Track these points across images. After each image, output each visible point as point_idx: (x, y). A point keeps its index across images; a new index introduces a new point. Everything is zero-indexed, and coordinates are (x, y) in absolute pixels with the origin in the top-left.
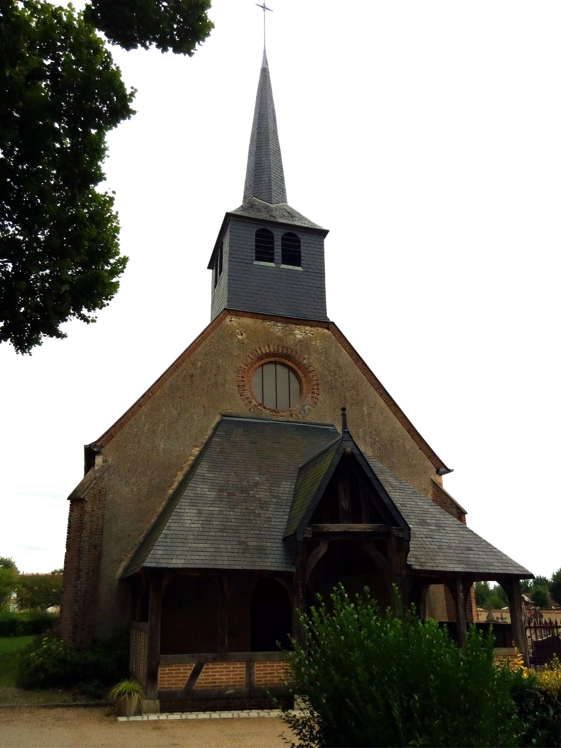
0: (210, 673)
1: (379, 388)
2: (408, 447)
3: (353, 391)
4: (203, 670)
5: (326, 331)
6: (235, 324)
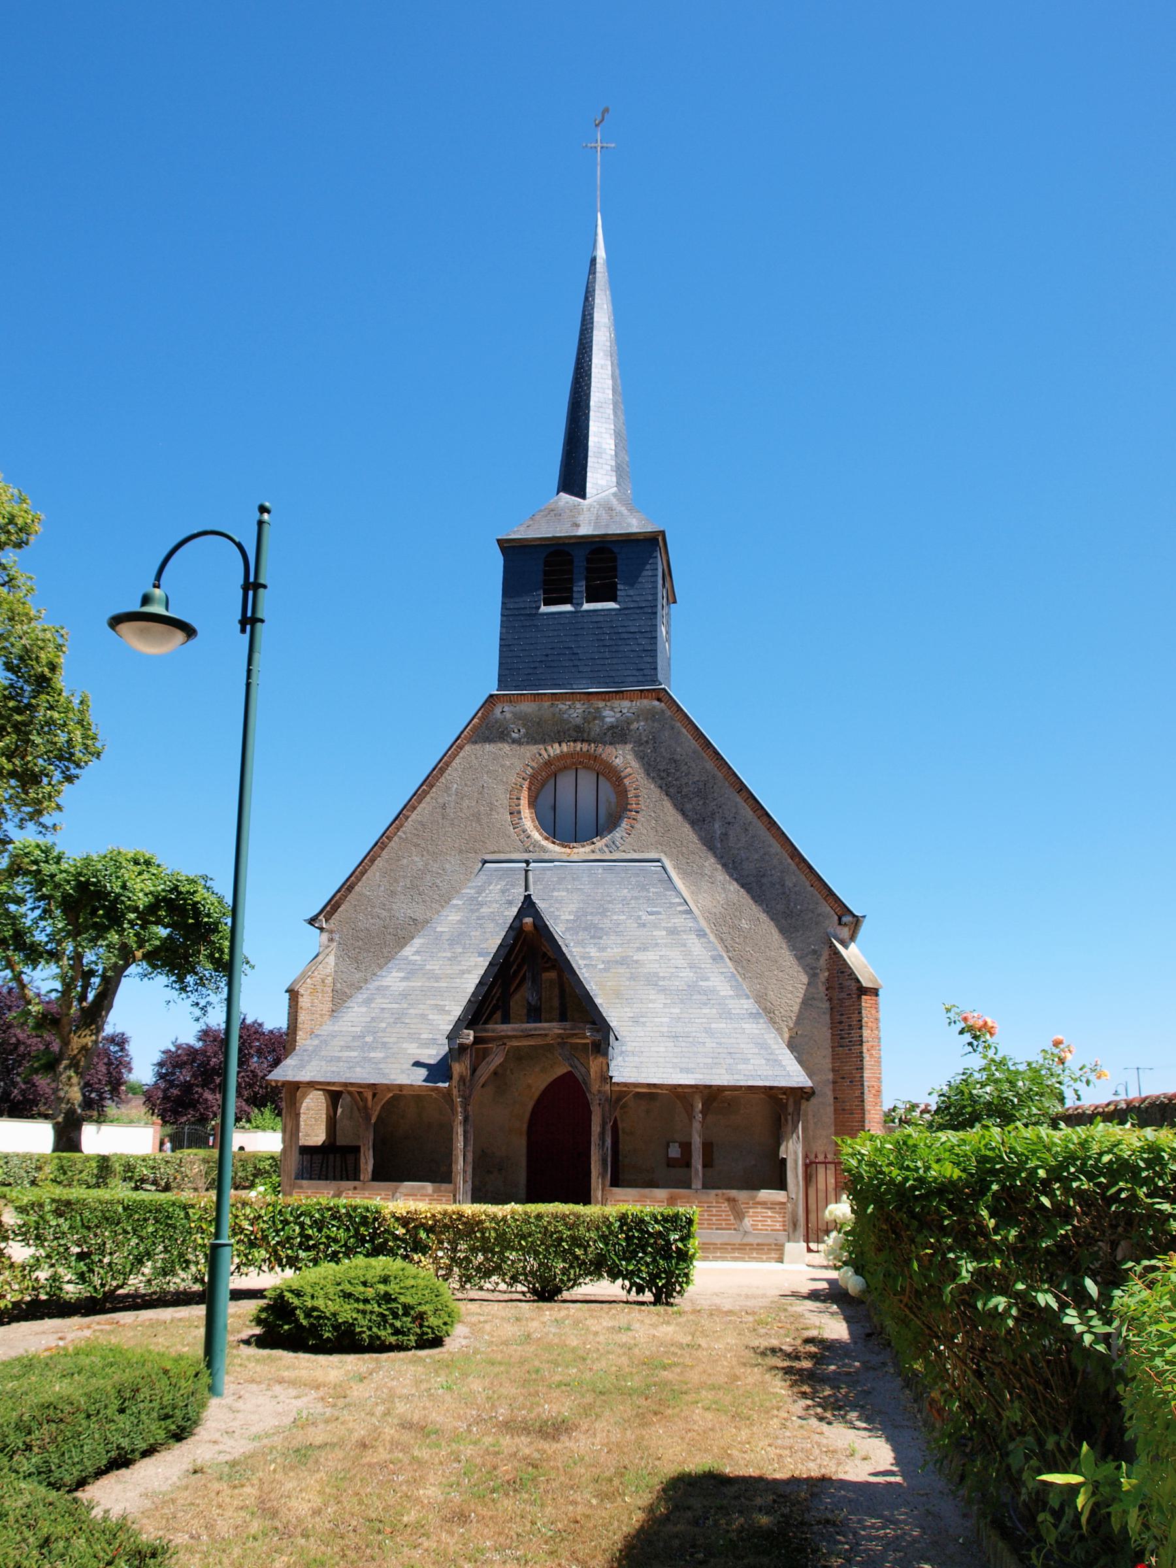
2: (789, 884)
5: (656, 703)
6: (508, 716)
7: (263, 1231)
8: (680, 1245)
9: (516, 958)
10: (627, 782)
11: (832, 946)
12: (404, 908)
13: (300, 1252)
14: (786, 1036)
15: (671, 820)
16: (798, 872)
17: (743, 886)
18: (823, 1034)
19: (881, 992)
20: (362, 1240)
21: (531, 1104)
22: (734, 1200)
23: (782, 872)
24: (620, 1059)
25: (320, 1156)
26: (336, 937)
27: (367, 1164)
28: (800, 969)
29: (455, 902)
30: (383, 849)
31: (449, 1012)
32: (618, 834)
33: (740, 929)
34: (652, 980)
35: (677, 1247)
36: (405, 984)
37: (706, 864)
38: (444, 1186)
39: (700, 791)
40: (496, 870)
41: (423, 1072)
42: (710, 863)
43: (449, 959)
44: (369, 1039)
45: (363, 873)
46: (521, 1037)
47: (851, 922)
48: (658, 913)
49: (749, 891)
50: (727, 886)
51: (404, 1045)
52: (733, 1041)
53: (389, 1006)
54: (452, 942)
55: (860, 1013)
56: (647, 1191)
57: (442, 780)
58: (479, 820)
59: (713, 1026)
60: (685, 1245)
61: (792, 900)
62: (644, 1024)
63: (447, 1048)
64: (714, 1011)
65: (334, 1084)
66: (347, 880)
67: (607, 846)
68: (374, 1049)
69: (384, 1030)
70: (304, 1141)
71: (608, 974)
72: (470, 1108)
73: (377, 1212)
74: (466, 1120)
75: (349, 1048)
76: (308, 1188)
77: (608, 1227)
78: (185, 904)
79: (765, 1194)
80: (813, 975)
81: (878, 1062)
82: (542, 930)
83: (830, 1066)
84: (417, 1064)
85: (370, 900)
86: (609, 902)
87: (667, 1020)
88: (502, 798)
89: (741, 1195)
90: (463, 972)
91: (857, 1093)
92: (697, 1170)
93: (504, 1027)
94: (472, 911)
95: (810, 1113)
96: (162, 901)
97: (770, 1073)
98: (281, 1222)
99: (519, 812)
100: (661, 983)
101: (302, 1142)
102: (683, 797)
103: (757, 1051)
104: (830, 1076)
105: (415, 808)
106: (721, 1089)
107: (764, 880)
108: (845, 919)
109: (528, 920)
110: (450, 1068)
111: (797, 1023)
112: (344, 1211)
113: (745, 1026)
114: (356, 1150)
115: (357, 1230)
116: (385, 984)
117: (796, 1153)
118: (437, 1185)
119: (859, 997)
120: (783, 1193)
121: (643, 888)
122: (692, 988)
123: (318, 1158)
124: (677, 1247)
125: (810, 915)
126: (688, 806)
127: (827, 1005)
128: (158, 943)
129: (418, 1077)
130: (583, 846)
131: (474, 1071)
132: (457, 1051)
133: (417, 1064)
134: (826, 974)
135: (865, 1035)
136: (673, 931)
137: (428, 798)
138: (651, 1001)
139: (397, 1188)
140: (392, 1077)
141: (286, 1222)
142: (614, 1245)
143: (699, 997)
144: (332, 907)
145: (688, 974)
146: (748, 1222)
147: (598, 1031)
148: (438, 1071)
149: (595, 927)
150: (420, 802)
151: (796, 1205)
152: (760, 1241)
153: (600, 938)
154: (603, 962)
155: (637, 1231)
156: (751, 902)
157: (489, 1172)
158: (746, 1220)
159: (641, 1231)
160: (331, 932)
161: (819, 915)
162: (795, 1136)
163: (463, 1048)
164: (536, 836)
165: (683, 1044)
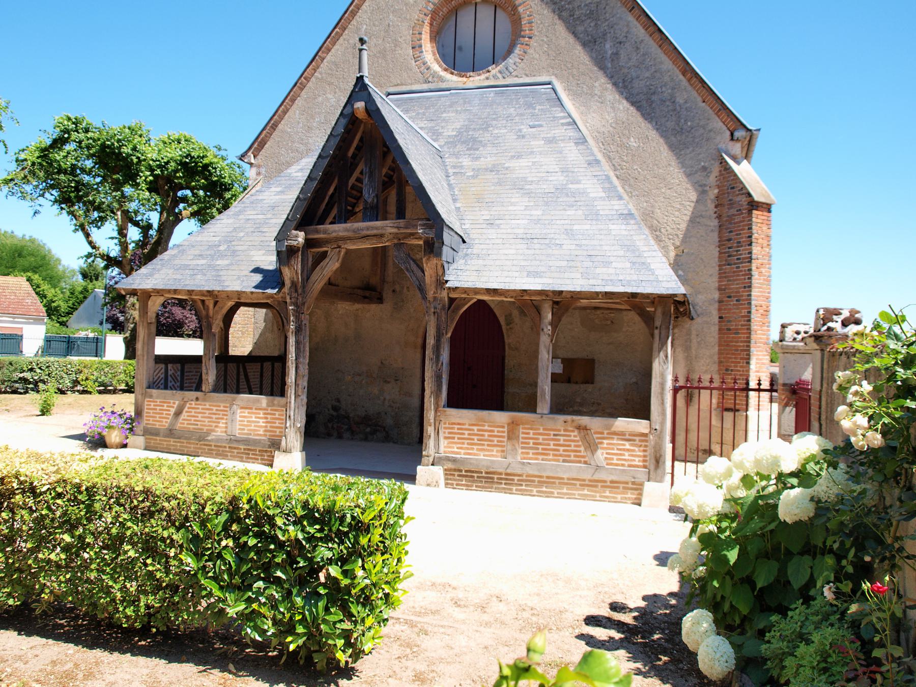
2: (680, 100)
4: (186, 409)
8: (335, 571)
10: (521, 9)
11: (723, 162)
14: (672, 254)
15: (563, 43)
16: (690, 88)
18: (712, 252)
19: (773, 209)
22: (586, 428)
23: (673, 89)
25: (179, 366)
26: (263, 170)
28: (689, 186)
30: (302, 89)
32: (510, 60)
33: (628, 148)
34: (520, 186)
35: (328, 576)
37: (597, 84)
38: (278, 400)
39: (592, 12)
42: (601, 83)
45: (285, 113)
47: (745, 138)
48: (541, 126)
49: (639, 108)
50: (616, 105)
52: (595, 242)
53: (255, 217)
57: (354, 22)
58: (384, 57)
59: (575, 227)
60: (345, 573)
61: (683, 112)
62: (498, 226)
64: (580, 212)
66: (271, 119)
67: (500, 72)
71: (475, 181)
77: (203, 524)
79: (623, 423)
80: (702, 191)
81: (768, 280)
83: (717, 285)
84: (257, 270)
86: (494, 119)
87: (526, 222)
88: (406, 34)
89: (594, 423)
91: (744, 312)
92: (543, 391)
95: (694, 333)
97: (635, 277)
99: (420, 46)
101: (157, 353)
102: (574, 20)
103: (621, 253)
104: (716, 295)
105: (329, 50)
106: (575, 296)
107: (654, 98)
108: (737, 134)
109: (360, 105)
111: (684, 240)
113: (612, 227)
121: (530, 106)
122: (561, 190)
124: (328, 576)
125: (701, 131)
126: (580, 29)
127: (715, 223)
130: (479, 75)
131: (307, 278)
134: (716, 191)
135: (754, 252)
136: (551, 141)
137: (341, 41)
138: (512, 204)
140: (226, 284)
143: (565, 199)
145: (560, 178)
147: (430, 227)
149: (474, 140)
150: (334, 44)
151: (660, 437)
152: (615, 478)
153: (477, 149)
155: (256, 535)
156: (640, 119)
157: (387, 382)
158: (599, 452)
160: (259, 166)
161: (710, 131)
162: (662, 354)
164: (436, 67)
165: (537, 246)
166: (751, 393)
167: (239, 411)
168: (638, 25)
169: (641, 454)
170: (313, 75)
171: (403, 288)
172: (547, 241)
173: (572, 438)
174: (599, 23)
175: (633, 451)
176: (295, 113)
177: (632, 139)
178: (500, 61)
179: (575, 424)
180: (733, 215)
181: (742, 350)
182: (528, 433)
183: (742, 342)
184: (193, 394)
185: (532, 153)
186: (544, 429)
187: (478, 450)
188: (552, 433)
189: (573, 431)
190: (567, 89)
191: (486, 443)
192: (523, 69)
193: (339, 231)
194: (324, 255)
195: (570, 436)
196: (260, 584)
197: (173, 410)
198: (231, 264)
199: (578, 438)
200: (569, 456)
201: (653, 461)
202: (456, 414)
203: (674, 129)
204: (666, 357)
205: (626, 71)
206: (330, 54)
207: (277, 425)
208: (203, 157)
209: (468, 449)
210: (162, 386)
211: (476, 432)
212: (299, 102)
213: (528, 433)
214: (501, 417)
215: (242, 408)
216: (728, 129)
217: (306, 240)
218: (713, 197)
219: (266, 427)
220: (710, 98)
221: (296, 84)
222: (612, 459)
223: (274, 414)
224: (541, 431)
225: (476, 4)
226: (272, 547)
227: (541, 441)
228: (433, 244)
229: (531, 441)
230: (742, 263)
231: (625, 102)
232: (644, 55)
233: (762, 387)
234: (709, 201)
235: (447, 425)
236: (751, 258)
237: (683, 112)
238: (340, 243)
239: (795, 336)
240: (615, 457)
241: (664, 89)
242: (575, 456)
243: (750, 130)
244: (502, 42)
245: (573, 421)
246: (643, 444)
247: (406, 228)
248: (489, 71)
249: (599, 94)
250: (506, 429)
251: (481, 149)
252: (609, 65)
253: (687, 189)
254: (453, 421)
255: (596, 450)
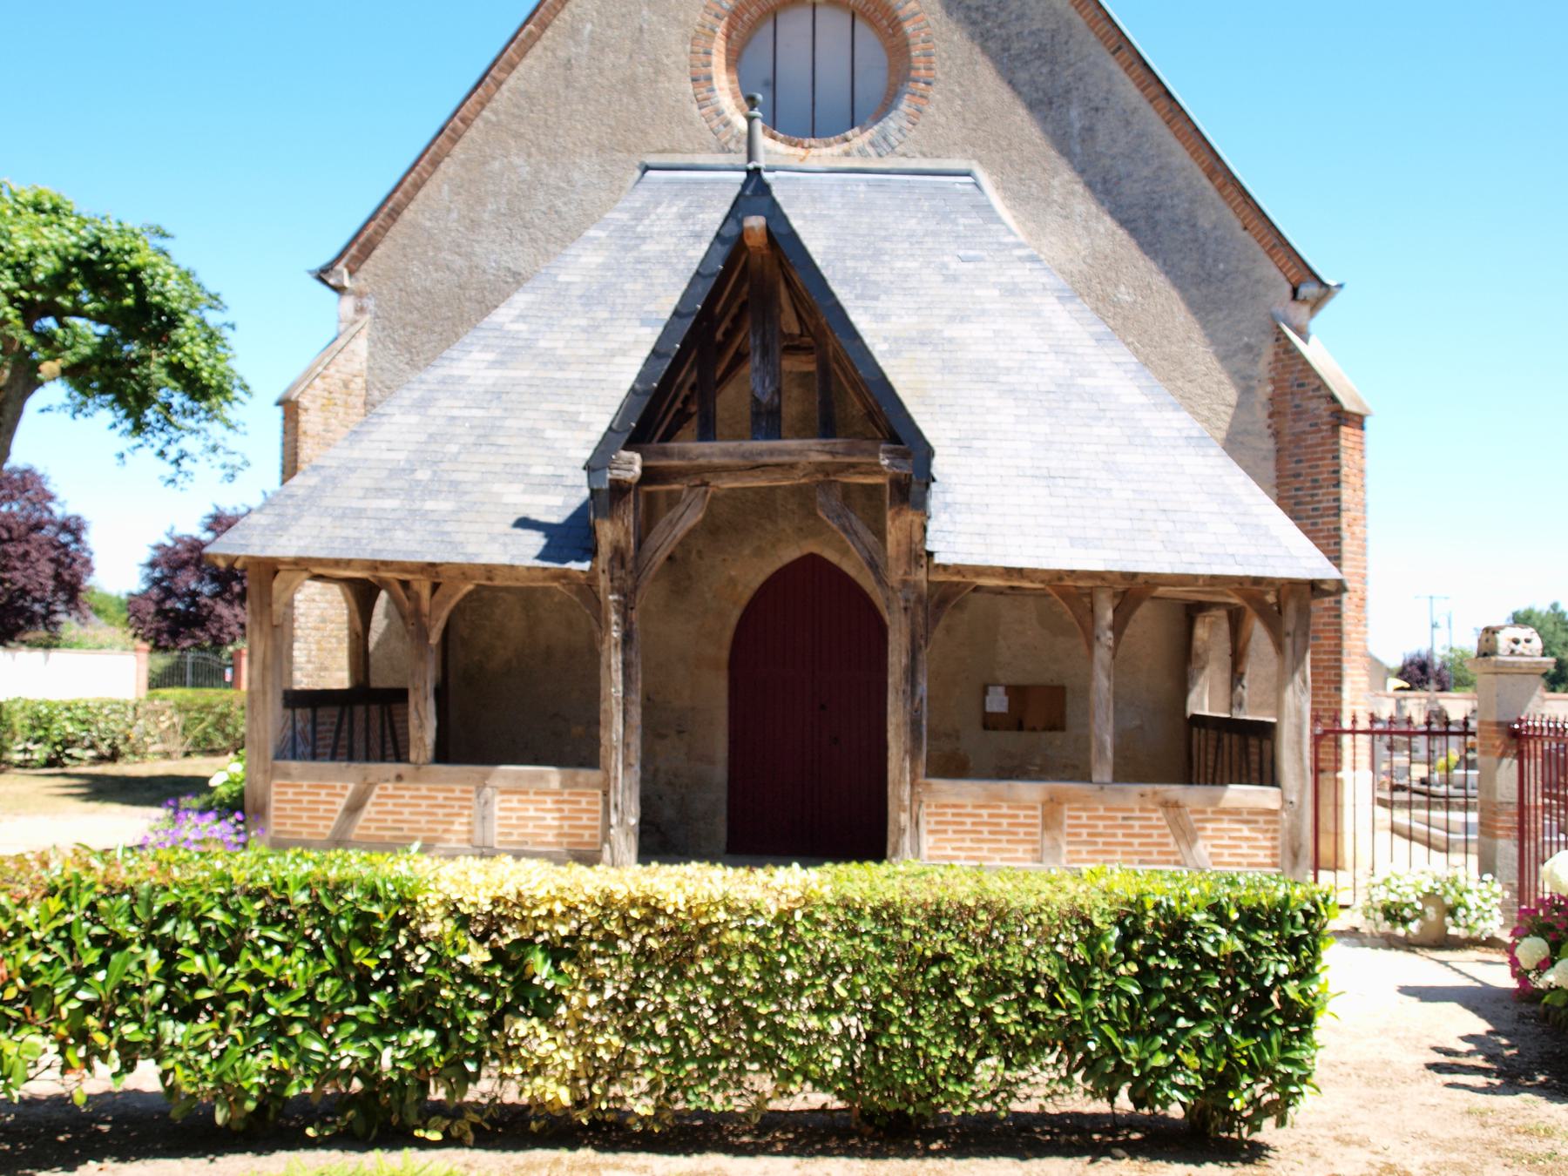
0: (390, 808)
1: (1119, 48)
2: (1204, 223)
3: (1038, 63)
4: (373, 799)
7: (28, 974)
9: (727, 305)
10: (909, 28)
11: (1281, 337)
12: (493, 253)
13: (168, 1026)
15: (990, 99)
16: (1221, 203)
17: (1123, 223)
19: (1368, 422)
20: (363, 986)
21: (735, 615)
22: (1176, 805)
23: (1192, 202)
24: (944, 517)
25: (336, 711)
26: (370, 304)
27: (423, 727)
28: (1223, 377)
29: (591, 233)
30: (454, 141)
31: (587, 426)
32: (892, 123)
33: (1116, 304)
36: (497, 373)
37: (1056, 182)
38: (584, 774)
39: (1043, 48)
40: (668, 182)
41: (537, 540)
42: (1064, 180)
43: (584, 330)
44: (423, 475)
45: (418, 186)
46: (740, 469)
48: (981, 259)
49: (1133, 232)
50: (1093, 224)
51: (497, 487)
53: (466, 413)
54: (588, 300)
55: (1337, 457)
56: (1001, 786)
57: (565, 15)
58: (633, 92)
61: (1210, 252)
63: (586, 493)
65: (348, 563)
66: (389, 197)
67: (872, 144)
68: (432, 494)
69: (454, 458)
70: (304, 680)
72: (634, 615)
73: (402, 901)
74: (627, 639)
75: (380, 491)
76: (302, 777)
78: (114, 271)
79: (1238, 794)
80: (1246, 391)
82: (783, 245)
84: (524, 523)
85: (431, 237)
86: (885, 239)
88: (677, 53)
90: (613, 354)
93: (706, 447)
94: (626, 249)
96: (73, 264)
98: (97, 941)
99: (709, 79)
100: (1003, 379)
105: (513, 66)
108: (1304, 291)
109: (756, 222)
110: (592, 532)
112: (303, 898)
114: (401, 695)
115: (343, 957)
116: (456, 372)
117: (1299, 712)
118: (569, 771)
119: (1335, 429)
120: (1272, 791)
123: (328, 715)
126: (1022, 76)
127: (1269, 445)
128: (87, 351)
129: (526, 550)
130: (828, 145)
132: (608, 497)
133: (524, 523)
134: (1270, 388)
137: (538, 49)
139: (485, 777)
140: (471, 549)
141: (111, 944)
142: (1105, 994)
144: (360, 248)
146: (1202, 848)
147: (905, 455)
148: (568, 538)
150: (523, 54)
151: (1298, 815)
153: (876, 298)
154: (886, 339)
155: (1171, 953)
156: (1136, 253)
158: (1200, 844)
159: (1186, 955)
160: (360, 295)
161: (1258, 282)
162: (1297, 678)
163: (619, 490)
166: (1346, 740)
167: (498, 798)
168: (1128, 80)
169: (1268, 844)
170: (477, 114)
171: (689, 552)
172: (1081, 483)
173: (1154, 822)
174: (1057, 68)
175: (1255, 839)
176: (438, 188)
177: (1122, 288)
178: (868, 122)
179: (1159, 798)
180: (1304, 432)
181: (1326, 668)
182: (1078, 818)
183: (1325, 652)
184: (391, 768)
185: (983, 312)
186: (1106, 809)
187: (990, 850)
188: (1120, 815)
189: (1155, 811)
190: (1002, 187)
191: (1004, 837)
192: (916, 142)
193: (712, 455)
194: (673, 500)
195: (1149, 819)
196: (1182, 1022)
197: (341, 804)
198: (461, 510)
199: (1163, 823)
200: (1150, 853)
201: (1289, 855)
202: (947, 789)
203: (1195, 275)
204: (1305, 682)
205: (1107, 162)
206: (515, 74)
207: (585, 822)
208: (130, 252)
209: (972, 849)
210: (289, 754)
211: (986, 819)
212: (448, 167)
213: (1078, 818)
214: (1031, 792)
215: (504, 792)
216: (1288, 280)
217: (644, 469)
218: (1264, 399)
219: (561, 827)
220: (1256, 223)
221: (441, 131)
222: (1221, 855)
223: (578, 802)
224: (1101, 813)
225: (814, 6)
226: (1197, 967)
227: (1101, 830)
228: (908, 485)
229: (1084, 831)
230: (1322, 516)
231: (1107, 219)
232: (1139, 136)
233: (1359, 728)
234: (1258, 407)
235: (933, 810)
236: (1338, 508)
237: (1210, 252)
238: (707, 477)
239: (1513, 646)
240: (1226, 852)
241: (1176, 201)
242: (1160, 853)
243: (1327, 286)
244: (872, 81)
245: (1155, 793)
246: (1271, 827)
247: (848, 453)
248: (846, 140)
249: (1060, 200)
250: (1039, 813)
251: (883, 297)
252: (1078, 149)
253: (1220, 383)
254: (945, 801)
255: (1194, 840)
